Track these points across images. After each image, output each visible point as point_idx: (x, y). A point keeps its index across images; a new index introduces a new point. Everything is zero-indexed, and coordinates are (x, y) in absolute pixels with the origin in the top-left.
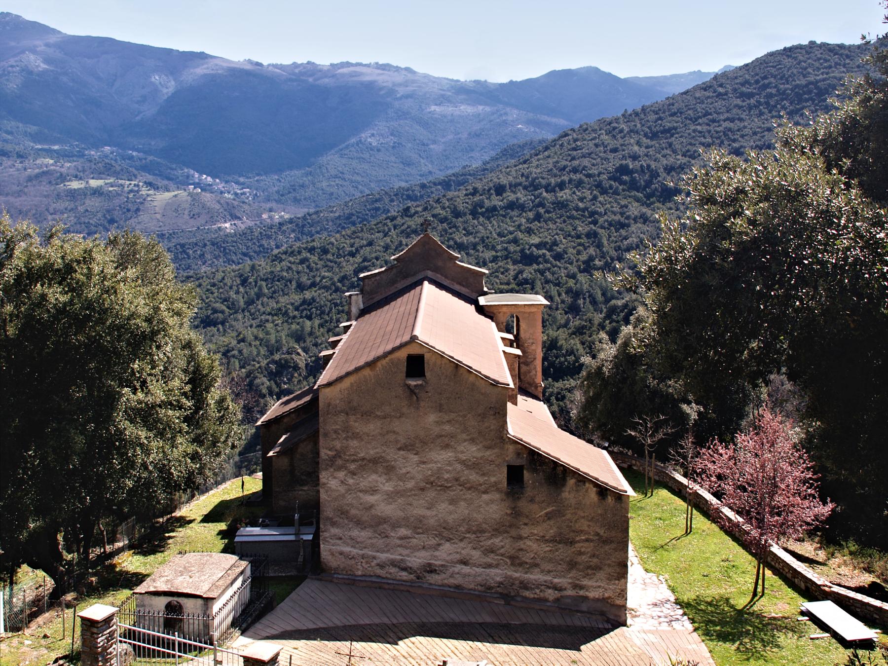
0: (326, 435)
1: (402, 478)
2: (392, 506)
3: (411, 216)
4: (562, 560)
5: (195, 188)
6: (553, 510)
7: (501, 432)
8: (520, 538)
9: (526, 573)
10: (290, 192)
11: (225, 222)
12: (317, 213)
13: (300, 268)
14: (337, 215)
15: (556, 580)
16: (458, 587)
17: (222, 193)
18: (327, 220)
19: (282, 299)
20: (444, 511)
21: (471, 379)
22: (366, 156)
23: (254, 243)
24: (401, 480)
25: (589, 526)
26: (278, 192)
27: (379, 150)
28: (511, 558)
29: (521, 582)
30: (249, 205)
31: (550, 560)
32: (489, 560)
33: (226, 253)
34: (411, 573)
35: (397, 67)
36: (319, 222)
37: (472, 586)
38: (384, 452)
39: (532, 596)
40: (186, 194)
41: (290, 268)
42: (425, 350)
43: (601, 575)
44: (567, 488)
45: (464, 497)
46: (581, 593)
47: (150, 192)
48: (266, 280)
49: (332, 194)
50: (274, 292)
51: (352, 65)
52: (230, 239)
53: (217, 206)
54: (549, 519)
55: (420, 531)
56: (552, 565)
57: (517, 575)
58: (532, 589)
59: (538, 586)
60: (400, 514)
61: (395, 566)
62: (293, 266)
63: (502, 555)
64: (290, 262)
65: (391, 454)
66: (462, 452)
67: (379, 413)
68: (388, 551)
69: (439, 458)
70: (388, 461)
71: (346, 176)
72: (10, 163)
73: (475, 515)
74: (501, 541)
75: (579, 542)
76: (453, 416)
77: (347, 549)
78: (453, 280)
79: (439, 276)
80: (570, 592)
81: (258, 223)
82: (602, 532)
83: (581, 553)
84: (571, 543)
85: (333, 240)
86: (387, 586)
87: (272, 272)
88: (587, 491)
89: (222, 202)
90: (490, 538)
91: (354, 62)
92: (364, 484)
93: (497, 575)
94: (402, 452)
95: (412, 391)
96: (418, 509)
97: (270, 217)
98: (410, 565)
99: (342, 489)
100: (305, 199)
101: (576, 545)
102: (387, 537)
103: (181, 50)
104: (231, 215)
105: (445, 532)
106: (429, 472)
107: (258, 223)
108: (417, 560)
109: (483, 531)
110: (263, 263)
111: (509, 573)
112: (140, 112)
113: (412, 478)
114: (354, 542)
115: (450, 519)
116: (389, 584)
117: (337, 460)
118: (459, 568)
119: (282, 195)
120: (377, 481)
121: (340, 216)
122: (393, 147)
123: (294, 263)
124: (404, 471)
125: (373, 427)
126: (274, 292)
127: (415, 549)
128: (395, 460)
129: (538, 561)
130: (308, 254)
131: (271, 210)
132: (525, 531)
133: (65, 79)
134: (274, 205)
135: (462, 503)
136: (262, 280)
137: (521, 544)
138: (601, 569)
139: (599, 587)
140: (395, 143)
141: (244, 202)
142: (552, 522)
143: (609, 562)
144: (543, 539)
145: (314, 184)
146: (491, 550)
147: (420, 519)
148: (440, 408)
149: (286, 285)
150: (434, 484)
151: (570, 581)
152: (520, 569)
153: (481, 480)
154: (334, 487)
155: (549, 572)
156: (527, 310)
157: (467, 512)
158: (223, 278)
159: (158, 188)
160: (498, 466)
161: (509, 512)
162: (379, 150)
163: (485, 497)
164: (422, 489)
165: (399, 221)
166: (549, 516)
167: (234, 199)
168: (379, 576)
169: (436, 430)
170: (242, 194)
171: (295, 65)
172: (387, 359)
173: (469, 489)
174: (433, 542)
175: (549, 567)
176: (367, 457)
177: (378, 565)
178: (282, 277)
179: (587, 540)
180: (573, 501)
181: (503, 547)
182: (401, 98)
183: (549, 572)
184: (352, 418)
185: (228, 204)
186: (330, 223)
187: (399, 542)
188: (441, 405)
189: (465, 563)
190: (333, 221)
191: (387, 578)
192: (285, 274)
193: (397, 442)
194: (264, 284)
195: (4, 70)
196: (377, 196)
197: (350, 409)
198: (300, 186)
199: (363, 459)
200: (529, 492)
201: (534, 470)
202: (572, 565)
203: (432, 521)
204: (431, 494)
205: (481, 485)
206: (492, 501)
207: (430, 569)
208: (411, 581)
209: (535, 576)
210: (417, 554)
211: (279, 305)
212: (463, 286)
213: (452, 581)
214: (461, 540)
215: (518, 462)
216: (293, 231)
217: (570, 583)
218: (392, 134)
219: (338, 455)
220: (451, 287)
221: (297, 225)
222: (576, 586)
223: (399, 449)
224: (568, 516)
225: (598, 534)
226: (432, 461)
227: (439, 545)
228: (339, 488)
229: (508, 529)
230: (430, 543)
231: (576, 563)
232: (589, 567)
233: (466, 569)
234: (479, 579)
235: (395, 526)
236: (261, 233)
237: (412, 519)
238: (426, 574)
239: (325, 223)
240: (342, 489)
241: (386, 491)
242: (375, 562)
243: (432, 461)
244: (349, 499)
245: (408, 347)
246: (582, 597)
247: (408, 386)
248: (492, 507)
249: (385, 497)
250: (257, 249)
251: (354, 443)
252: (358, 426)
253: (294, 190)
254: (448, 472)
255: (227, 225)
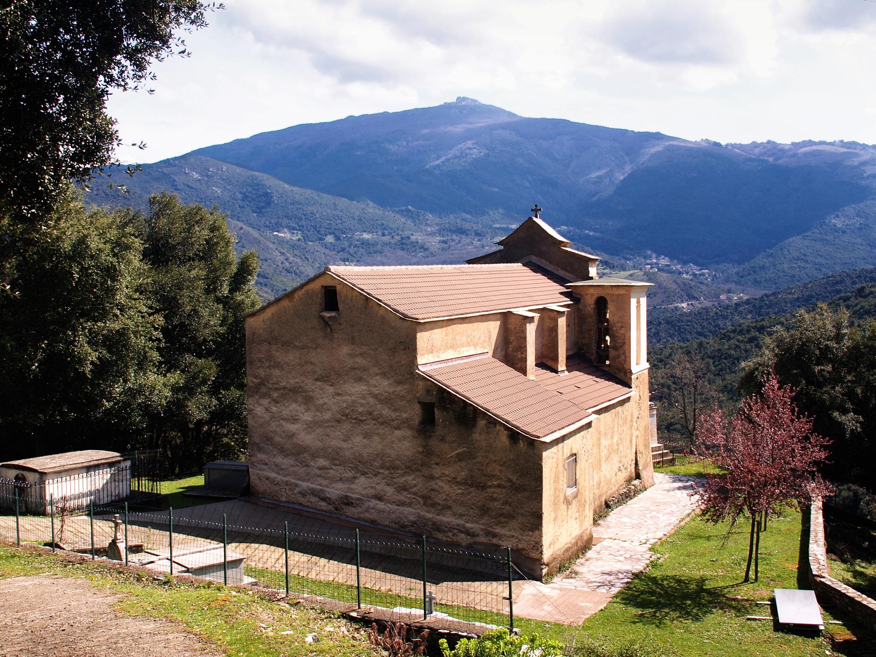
0: (252, 363)
1: (320, 409)
2: (312, 436)
3: (865, 297)
4: (473, 504)
5: (652, 268)
6: (464, 451)
7: (411, 367)
8: (432, 478)
9: (438, 514)
10: (749, 274)
11: (682, 302)
12: (774, 294)
13: (748, 346)
14: (795, 296)
15: (468, 525)
16: (373, 522)
17: (680, 273)
18: (785, 302)
19: (728, 377)
20: (358, 444)
21: (382, 312)
22: (830, 237)
23: (710, 323)
24: (319, 411)
25: (501, 471)
26: (737, 273)
27: (844, 232)
28: (423, 497)
29: (434, 524)
30: (707, 285)
31: (462, 504)
32: (402, 498)
33: (681, 332)
34: (329, 504)
35: (864, 144)
36: (777, 303)
37: (387, 523)
38: (303, 382)
39: (445, 539)
40: (642, 273)
41: (738, 346)
42: (337, 282)
43: (514, 524)
44: (478, 429)
45: (377, 431)
46: (494, 541)
47: (605, 271)
48: (713, 358)
49: (794, 276)
50: (721, 370)
51: (815, 143)
52: (685, 319)
53: (674, 286)
54: (460, 460)
55: (337, 462)
56: (464, 509)
57: (430, 516)
58: (446, 532)
59: (451, 529)
60: (319, 444)
61: (315, 495)
62: (741, 345)
63: (415, 494)
64: (738, 341)
65: (310, 385)
66: (375, 386)
67: (297, 344)
68: (308, 480)
69: (354, 390)
70: (307, 391)
71: (810, 259)
72: (468, 241)
73: (388, 451)
74: (414, 479)
75: (491, 487)
76: (365, 348)
77: (273, 475)
78: (557, 265)
79: (543, 261)
80: (482, 539)
81: (716, 303)
82: (514, 479)
83: (493, 499)
84: (483, 487)
85: (783, 319)
86: (306, 514)
87: (720, 350)
88: (498, 434)
89: (678, 281)
90: (403, 476)
91: (817, 140)
92: (286, 412)
93: (410, 513)
94: (319, 383)
95: (326, 323)
96: (335, 442)
97: (729, 299)
98: (328, 495)
99: (267, 416)
100: (765, 281)
101: (489, 490)
102: (307, 466)
103: (636, 131)
104: (688, 295)
105: (361, 466)
106: (345, 405)
107: (716, 303)
108: (335, 491)
109: (396, 468)
110: (711, 342)
111: (422, 513)
112: (596, 193)
113: (329, 410)
114: (278, 468)
115: (365, 453)
116: (308, 512)
117: (260, 389)
118: (373, 503)
119: (742, 277)
120: (297, 411)
121: (798, 298)
122: (860, 229)
123: (742, 341)
124: (321, 402)
125: (292, 357)
126: (721, 370)
127: (333, 480)
128: (313, 391)
129: (450, 503)
130: (757, 333)
131: (729, 291)
132: (437, 471)
133: (521, 160)
134: (733, 286)
135: (376, 438)
136: (710, 357)
137: (432, 484)
138: (513, 518)
139: (513, 536)
140: (861, 224)
141: (701, 283)
142: (463, 464)
143: (522, 511)
144: (454, 481)
145: (775, 266)
146: (403, 488)
147: (338, 451)
148: (352, 341)
149: (733, 363)
150: (348, 416)
151: (483, 527)
152: (433, 510)
153: (394, 415)
154: (259, 413)
155: (461, 515)
156: (616, 292)
157: (380, 447)
158: (670, 355)
159: (613, 267)
160: (408, 402)
161: (420, 450)
162: (844, 232)
163: (397, 433)
164: (338, 421)
165: (853, 301)
166: (460, 458)
167: (692, 280)
168: (301, 504)
169: (350, 362)
170: (700, 275)
171: (755, 145)
172: (303, 290)
173: (382, 424)
174: (350, 474)
175: (461, 510)
176: (288, 386)
177: (300, 493)
178: (729, 356)
179: (499, 486)
180: (484, 444)
181: (415, 486)
182: (868, 178)
183: (461, 515)
184: (274, 347)
185: (685, 284)
186: (789, 305)
187: (318, 472)
188: (353, 338)
189: (380, 498)
190: (791, 303)
191: (308, 507)
192: (733, 352)
193: (314, 372)
194: (711, 361)
195: (462, 153)
196: (839, 278)
197: (273, 339)
198: (760, 267)
199: (285, 388)
200: (440, 431)
201: (444, 409)
202: (484, 511)
203: (348, 454)
204: (347, 426)
205: (393, 420)
206: (405, 438)
207: (347, 501)
208: (330, 512)
209: (447, 519)
210: (335, 485)
211: (725, 382)
212: (568, 271)
213: (367, 515)
214: (375, 475)
215: (429, 399)
216: (750, 312)
217: (482, 530)
218: (858, 216)
219: (262, 383)
220: (555, 272)
221: (754, 306)
222: (488, 533)
223: (316, 380)
224: (479, 459)
225: (511, 481)
226: (346, 394)
227: (355, 478)
228: (265, 415)
229: (420, 467)
230: (346, 475)
231: (488, 509)
232: (502, 515)
233: (381, 505)
234: (393, 516)
235: (314, 456)
236: (716, 313)
237: (330, 450)
238: (343, 506)
239: (783, 304)
240: (267, 416)
241: (305, 421)
242: (297, 489)
243: (346, 394)
244: (273, 426)
245: (322, 278)
246: (495, 545)
247: (323, 318)
248: (403, 444)
249: (305, 426)
250: (713, 329)
251: (276, 372)
252: (279, 355)
253: (754, 272)
254: (362, 405)
255: (684, 305)
